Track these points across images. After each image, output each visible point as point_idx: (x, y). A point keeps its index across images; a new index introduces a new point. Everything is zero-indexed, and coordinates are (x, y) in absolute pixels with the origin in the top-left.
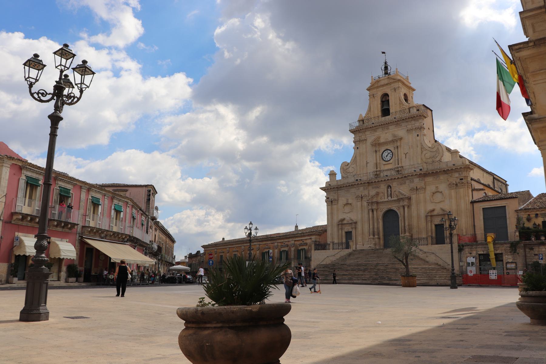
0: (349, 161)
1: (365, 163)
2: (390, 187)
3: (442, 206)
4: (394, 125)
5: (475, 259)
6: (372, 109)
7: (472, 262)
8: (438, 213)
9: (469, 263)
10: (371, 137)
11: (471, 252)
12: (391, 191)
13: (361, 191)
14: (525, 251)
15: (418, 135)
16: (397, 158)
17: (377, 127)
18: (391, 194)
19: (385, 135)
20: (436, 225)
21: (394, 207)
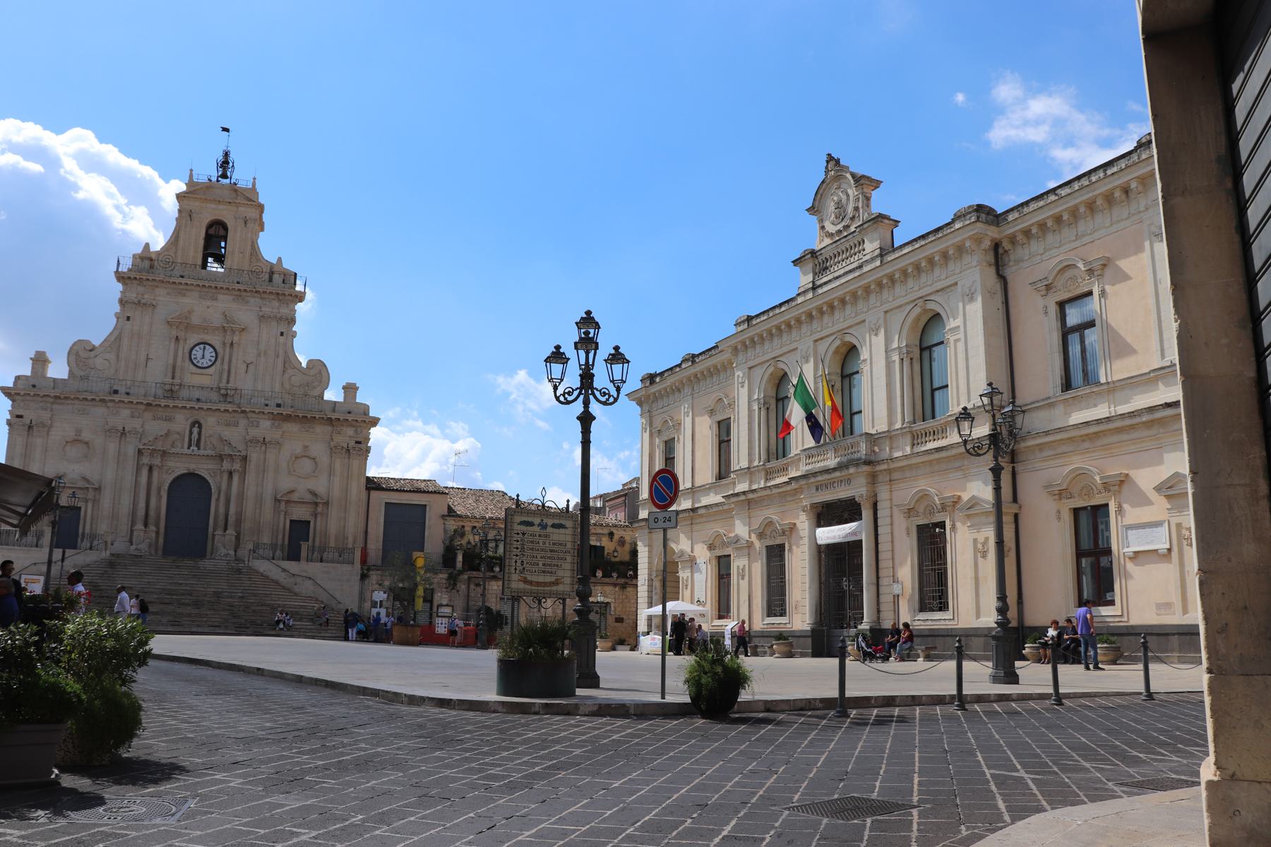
0: (97, 342)
1: (143, 358)
2: (197, 425)
3: (311, 484)
4: (232, 295)
5: (386, 595)
6: (181, 242)
7: (381, 601)
9: (377, 602)
10: (168, 303)
12: (200, 434)
13: (123, 417)
14: (469, 587)
15: (282, 334)
16: (226, 367)
17: (189, 288)
18: (199, 440)
19: (209, 310)
20: (292, 521)
21: (204, 469)
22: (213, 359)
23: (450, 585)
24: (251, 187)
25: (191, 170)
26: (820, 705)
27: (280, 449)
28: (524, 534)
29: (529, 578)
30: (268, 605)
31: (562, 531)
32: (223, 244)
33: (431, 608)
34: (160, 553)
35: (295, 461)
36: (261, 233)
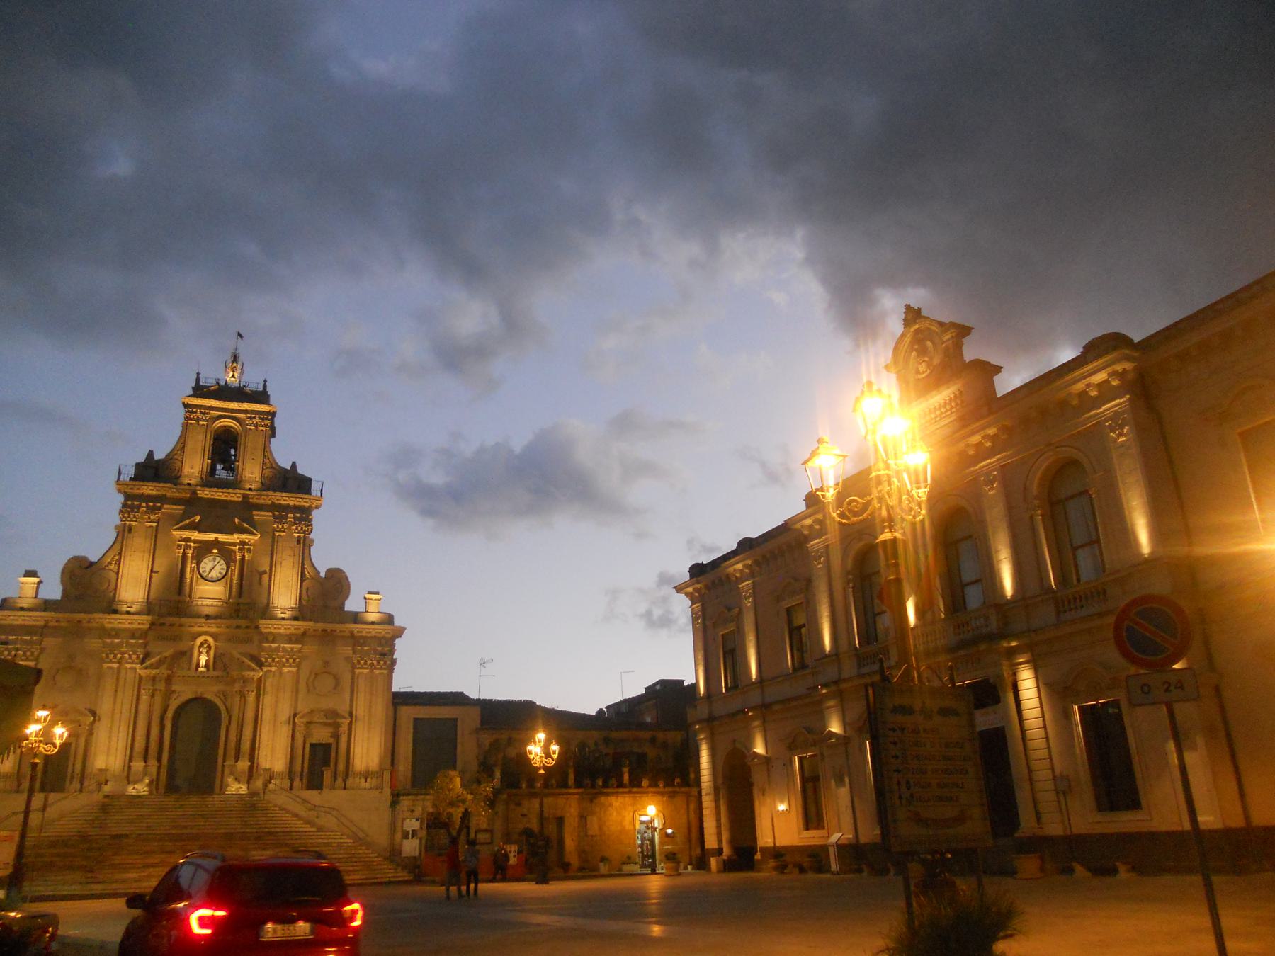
5: (418, 823)
8: (289, 723)
9: (408, 832)
11: (413, 808)
20: (312, 745)
22: (224, 572)
24: (262, 389)
25: (198, 374)
32: (233, 452)
34: (162, 790)
35: (315, 677)
36: (272, 440)
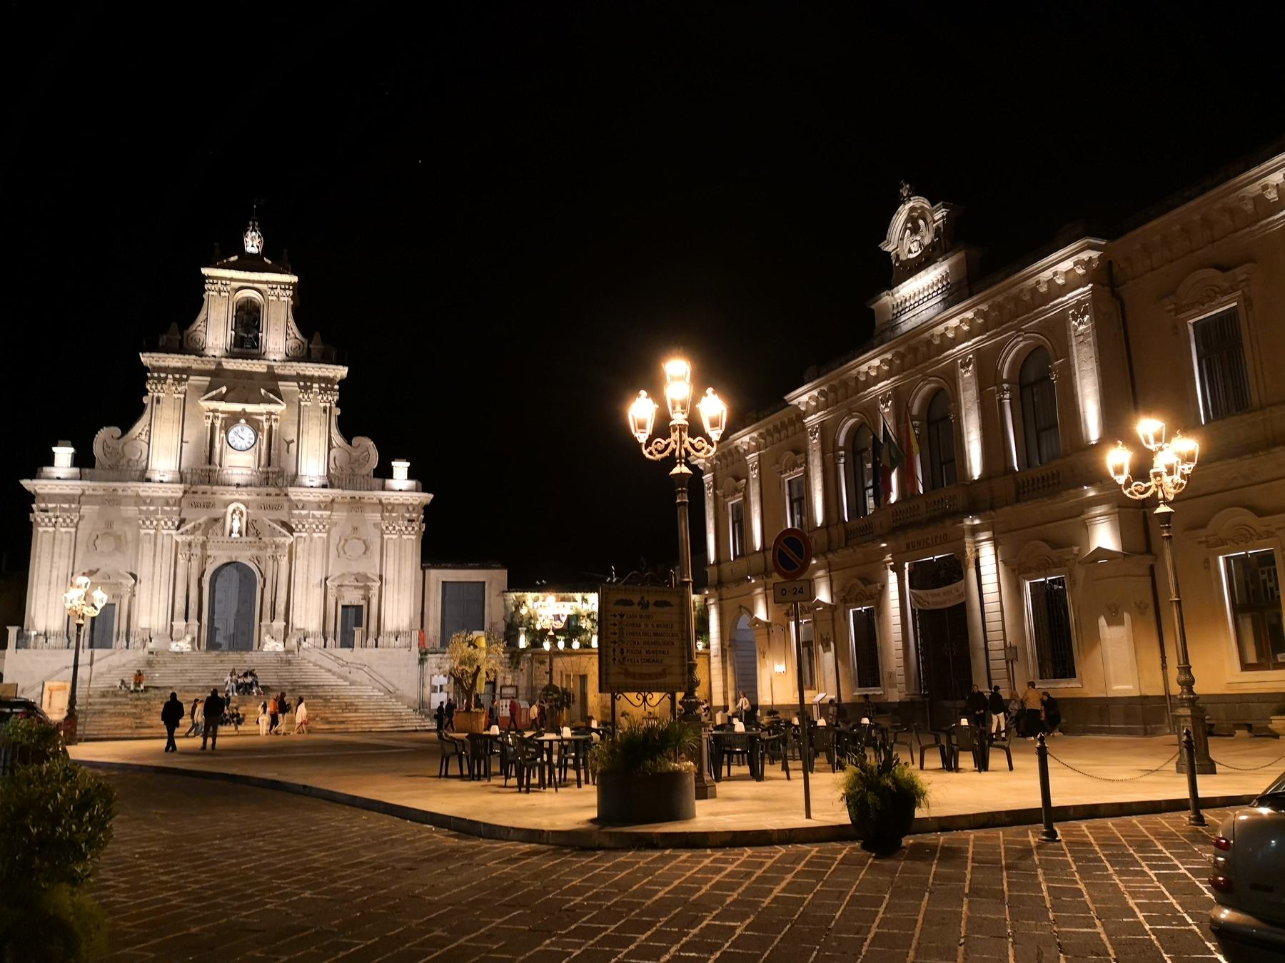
7: (441, 686)
9: (436, 687)
23: (512, 664)
26: (1007, 820)
27: (975, 771)
28: (622, 616)
29: (631, 669)
30: (321, 697)
31: (667, 609)
33: (494, 691)
34: (203, 647)
